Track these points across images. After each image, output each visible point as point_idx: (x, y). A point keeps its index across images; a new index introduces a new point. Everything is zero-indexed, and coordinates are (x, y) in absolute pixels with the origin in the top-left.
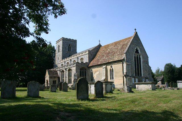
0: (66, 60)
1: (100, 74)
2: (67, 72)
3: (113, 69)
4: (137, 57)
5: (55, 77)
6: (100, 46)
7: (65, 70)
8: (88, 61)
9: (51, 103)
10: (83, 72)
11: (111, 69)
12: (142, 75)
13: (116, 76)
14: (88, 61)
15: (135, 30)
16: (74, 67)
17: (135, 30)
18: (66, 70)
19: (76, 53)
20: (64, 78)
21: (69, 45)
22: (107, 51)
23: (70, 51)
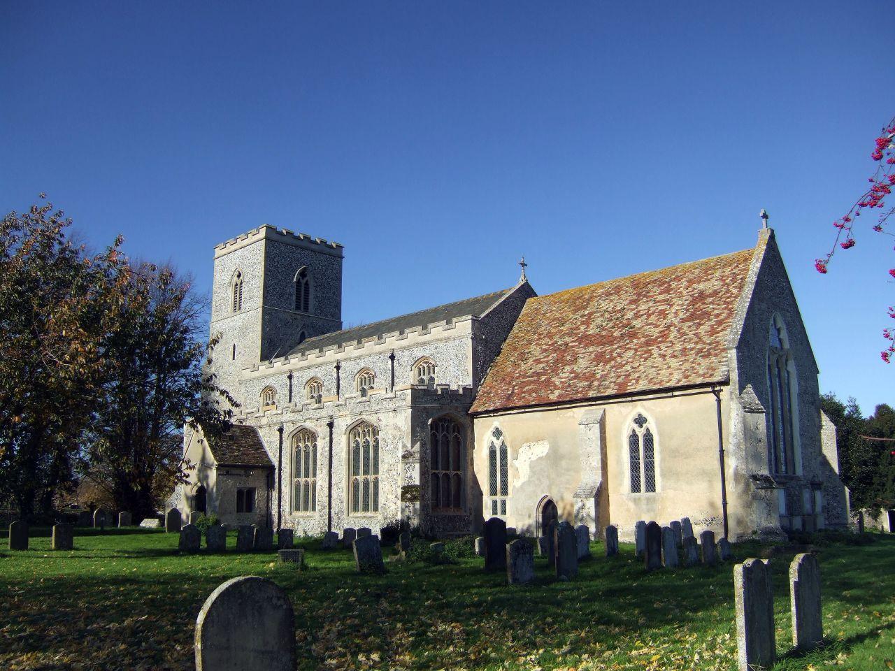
0: (295, 361)
1: (555, 457)
3: (649, 439)
5: (247, 468)
6: (526, 292)
8: (468, 381)
9: (859, 586)
11: (640, 432)
13: (667, 474)
14: (468, 381)
19: (339, 325)
20: (311, 471)
21: (239, 276)
22: (587, 323)
23: (306, 309)
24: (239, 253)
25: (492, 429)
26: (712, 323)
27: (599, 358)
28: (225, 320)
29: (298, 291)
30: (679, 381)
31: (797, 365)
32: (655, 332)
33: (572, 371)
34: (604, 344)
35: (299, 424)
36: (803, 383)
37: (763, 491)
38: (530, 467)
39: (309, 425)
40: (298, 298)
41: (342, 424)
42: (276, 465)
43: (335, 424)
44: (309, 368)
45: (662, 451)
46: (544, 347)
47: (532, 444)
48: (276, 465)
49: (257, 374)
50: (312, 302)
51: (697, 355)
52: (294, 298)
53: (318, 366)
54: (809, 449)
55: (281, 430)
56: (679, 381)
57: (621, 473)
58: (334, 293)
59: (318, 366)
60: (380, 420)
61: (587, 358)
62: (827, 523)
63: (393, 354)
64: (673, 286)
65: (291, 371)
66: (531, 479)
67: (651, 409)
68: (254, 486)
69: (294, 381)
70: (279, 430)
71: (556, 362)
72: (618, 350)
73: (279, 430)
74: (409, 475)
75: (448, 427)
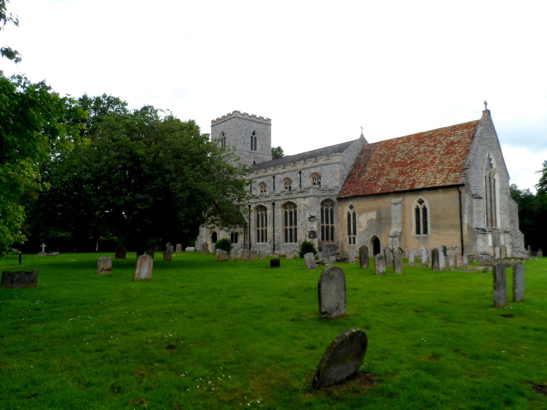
3: (425, 210)
7: (269, 206)
11: (421, 207)
12: (499, 226)
13: (434, 226)
15: (486, 104)
16: (304, 197)
17: (486, 104)
21: (254, 134)
23: (255, 149)
24: (223, 124)
29: (252, 141)
30: (440, 184)
35: (259, 204)
40: (252, 145)
41: (279, 204)
42: (248, 221)
45: (431, 216)
50: (258, 146)
52: (250, 145)
57: (411, 226)
60: (297, 202)
67: (428, 199)
74: (312, 226)
75: (328, 204)
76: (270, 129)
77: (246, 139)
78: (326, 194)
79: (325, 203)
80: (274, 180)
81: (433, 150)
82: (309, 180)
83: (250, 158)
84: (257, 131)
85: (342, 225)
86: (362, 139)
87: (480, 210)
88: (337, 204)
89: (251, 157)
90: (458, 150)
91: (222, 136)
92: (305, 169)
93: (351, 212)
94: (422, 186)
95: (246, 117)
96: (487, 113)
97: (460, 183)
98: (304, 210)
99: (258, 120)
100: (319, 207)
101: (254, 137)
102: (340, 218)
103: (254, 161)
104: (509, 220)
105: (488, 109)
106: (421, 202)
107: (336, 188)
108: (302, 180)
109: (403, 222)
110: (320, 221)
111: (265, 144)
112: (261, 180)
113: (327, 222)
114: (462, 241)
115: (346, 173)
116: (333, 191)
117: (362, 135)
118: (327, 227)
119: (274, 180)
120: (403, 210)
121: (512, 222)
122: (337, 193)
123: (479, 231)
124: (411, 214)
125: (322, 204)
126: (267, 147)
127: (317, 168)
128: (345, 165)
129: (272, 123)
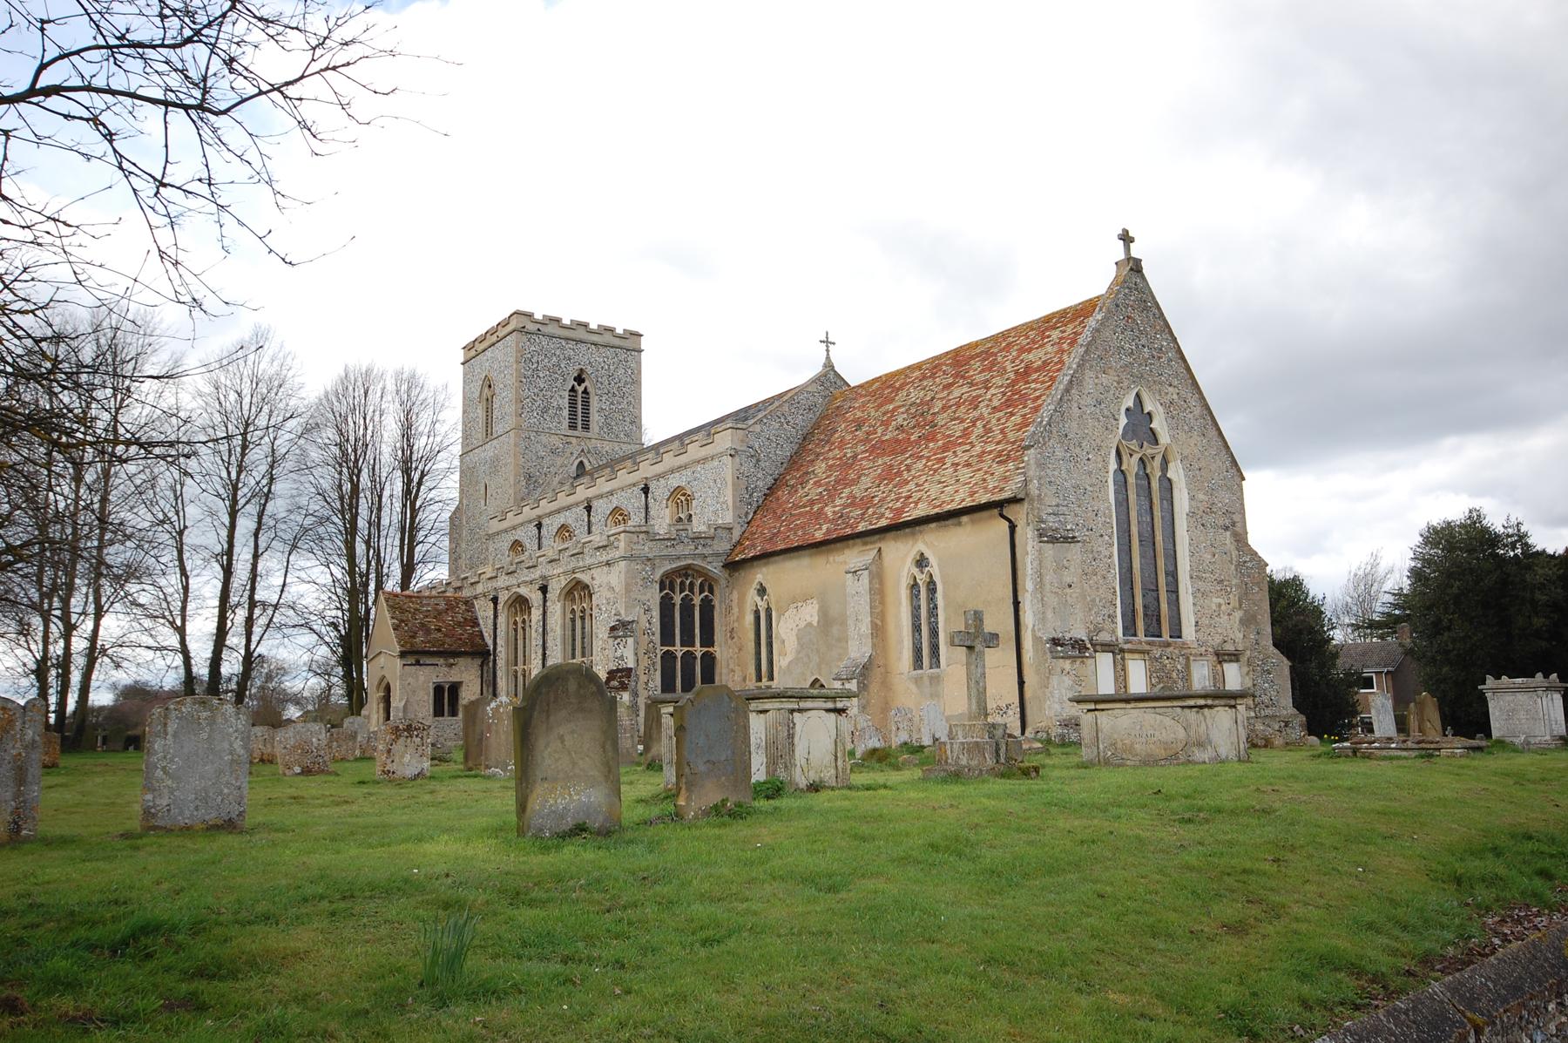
1: (827, 621)
2: (556, 609)
3: (932, 587)
4: (687, 607)
7: (535, 597)
10: (687, 607)
11: (922, 579)
18: (544, 589)
21: (579, 379)
22: (886, 424)
23: (586, 427)
24: (488, 353)
25: (755, 585)
26: (1027, 410)
27: (889, 475)
28: (476, 451)
29: (573, 404)
30: (963, 500)
31: (1188, 469)
32: (957, 429)
33: (852, 496)
34: (894, 452)
36: (1201, 496)
37: (1068, 662)
38: (798, 639)
39: (523, 591)
40: (573, 413)
41: (555, 588)
43: (549, 588)
44: (558, 511)
46: (831, 462)
47: (800, 604)
48: (490, 642)
49: (505, 525)
50: (595, 417)
51: (993, 460)
52: (566, 413)
53: (568, 508)
54: (1214, 599)
55: (495, 600)
56: (963, 500)
57: (900, 642)
58: (629, 403)
59: (568, 508)
61: (872, 475)
62: (1253, 714)
63: (646, 485)
64: (999, 359)
65: (540, 517)
66: (800, 655)
68: (459, 680)
69: (544, 531)
70: (540, 589)
71: (837, 482)
72: (909, 461)
73: (540, 589)
74: (618, 654)
75: (692, 584)
76: (639, 363)
77: (552, 397)
78: (680, 550)
79: (679, 581)
80: (589, 515)
81: (980, 396)
82: (667, 511)
83: (568, 454)
84: (589, 370)
85: (740, 650)
86: (829, 378)
87: (1069, 580)
88: (723, 582)
89: (569, 451)
90: (1035, 390)
91: (486, 389)
92: (659, 476)
93: (762, 605)
94: (921, 511)
95: (607, 338)
96: (1133, 267)
97: (1006, 495)
98: (608, 603)
99: (595, 338)
100: (654, 596)
101: (580, 389)
102: (736, 625)
103: (581, 462)
104: (1238, 614)
105: (1134, 254)
106: (921, 562)
107: (724, 534)
108: (652, 513)
109: (879, 631)
110: (657, 638)
111: (621, 411)
112: (560, 520)
113: (688, 640)
114: (1021, 683)
115: (760, 484)
116: (709, 541)
117: (829, 365)
118: (689, 657)
119: (589, 515)
120: (878, 593)
121: (1248, 621)
122: (723, 546)
123: (1059, 648)
124: (900, 603)
125: (667, 583)
126: (627, 419)
127: (684, 472)
128: (758, 461)
129: (644, 343)
